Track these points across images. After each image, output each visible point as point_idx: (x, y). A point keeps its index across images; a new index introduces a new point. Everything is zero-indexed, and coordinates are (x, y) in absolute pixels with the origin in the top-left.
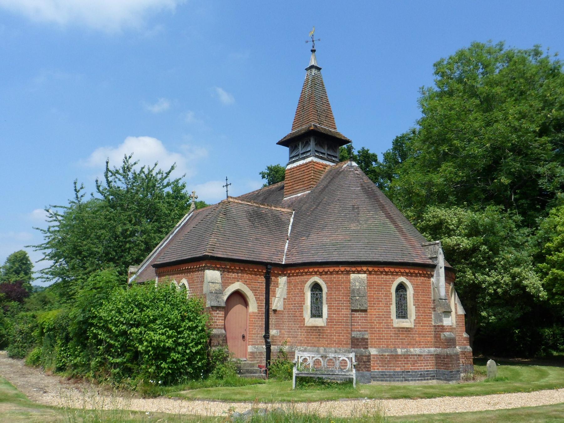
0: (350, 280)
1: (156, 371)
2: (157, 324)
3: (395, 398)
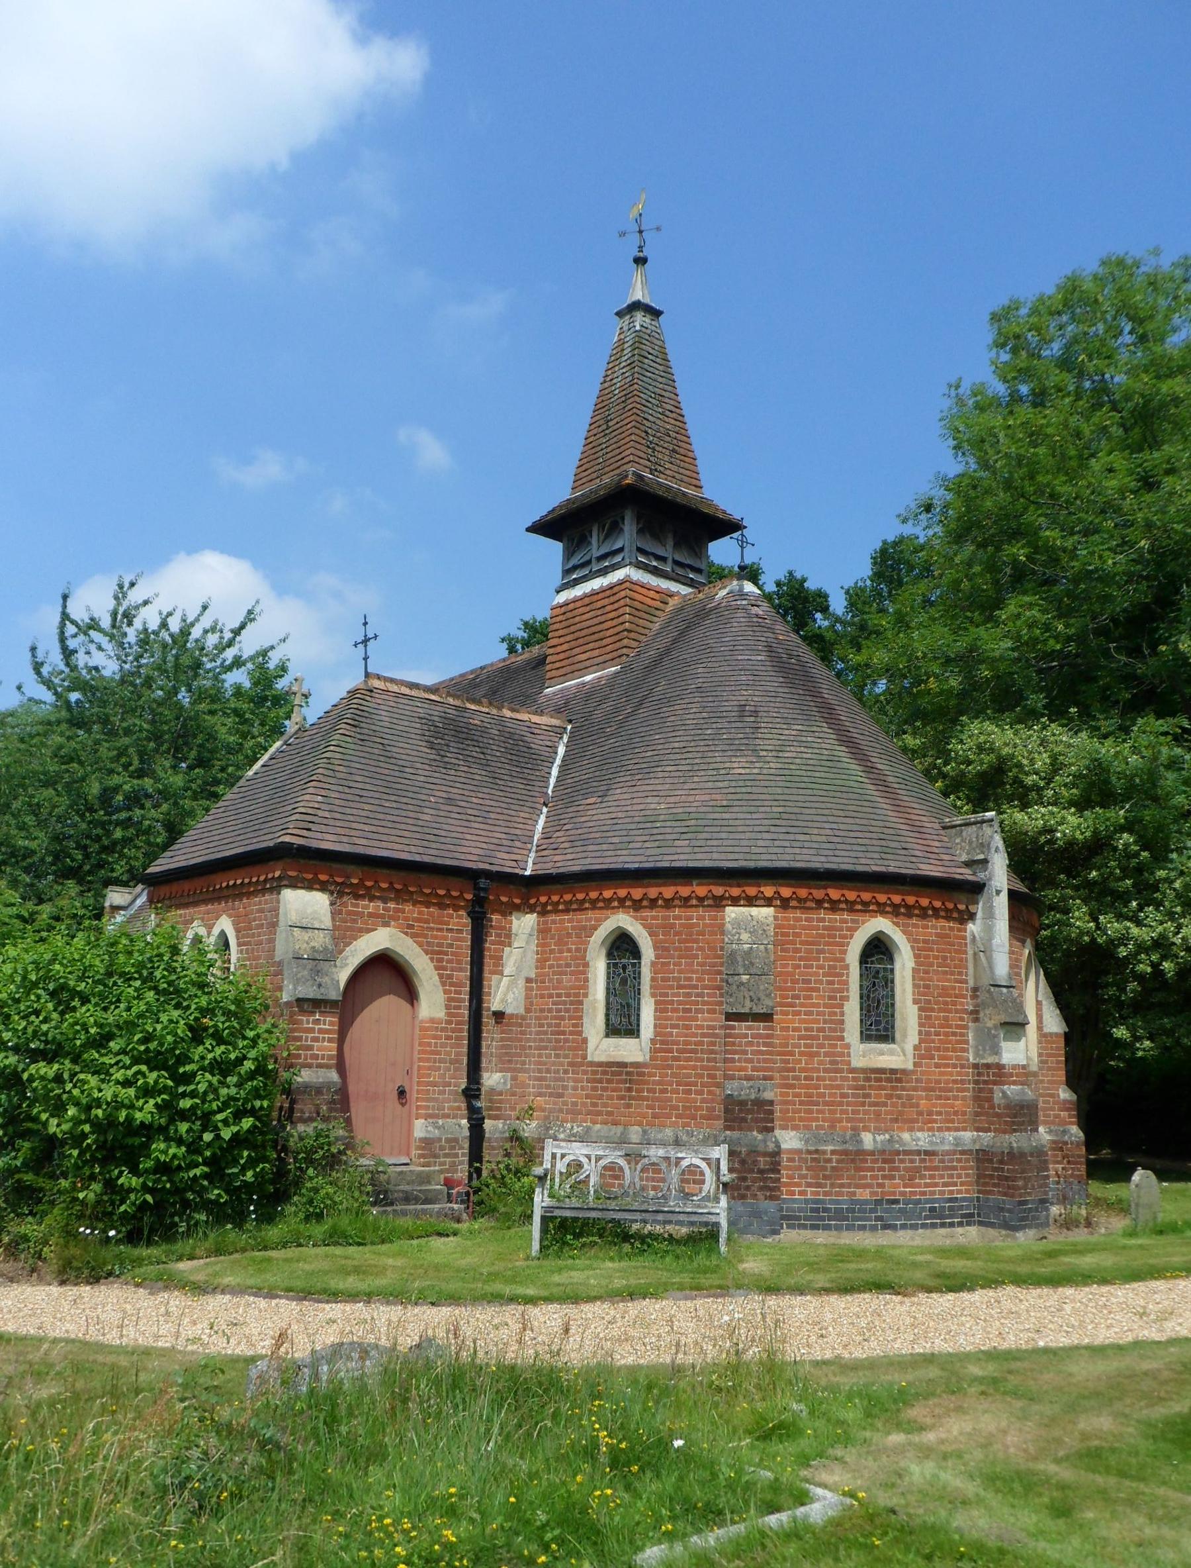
0: (723, 925)
1: (105, 1198)
2: (110, 1051)
3: (846, 1289)
